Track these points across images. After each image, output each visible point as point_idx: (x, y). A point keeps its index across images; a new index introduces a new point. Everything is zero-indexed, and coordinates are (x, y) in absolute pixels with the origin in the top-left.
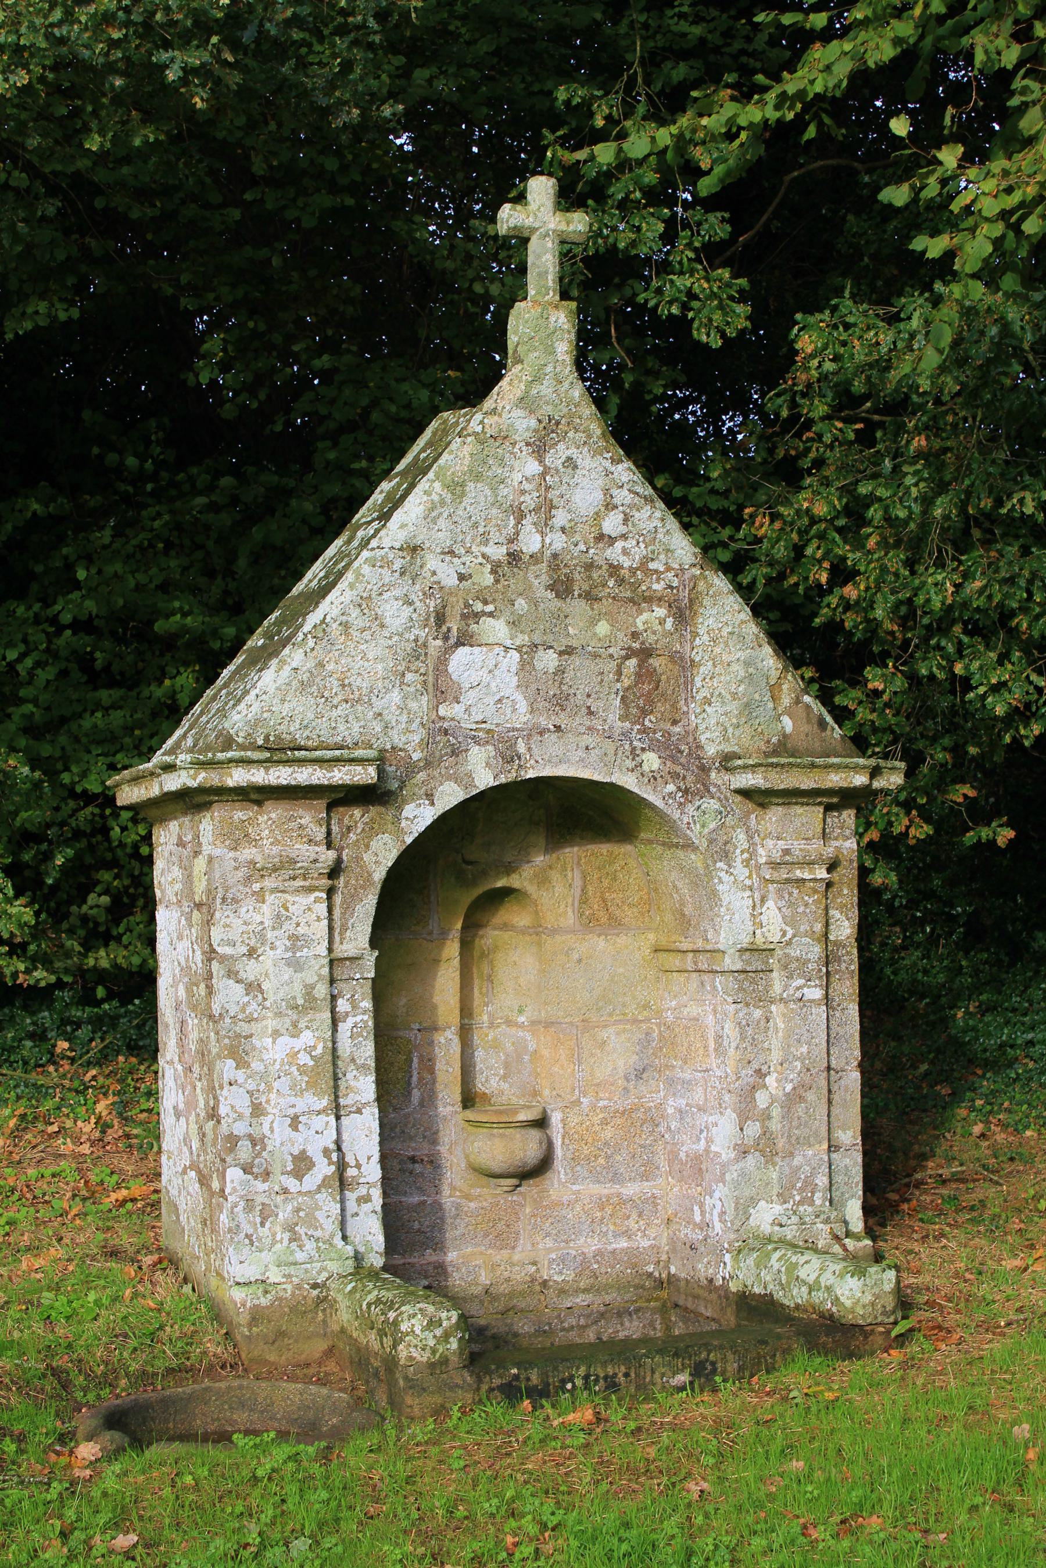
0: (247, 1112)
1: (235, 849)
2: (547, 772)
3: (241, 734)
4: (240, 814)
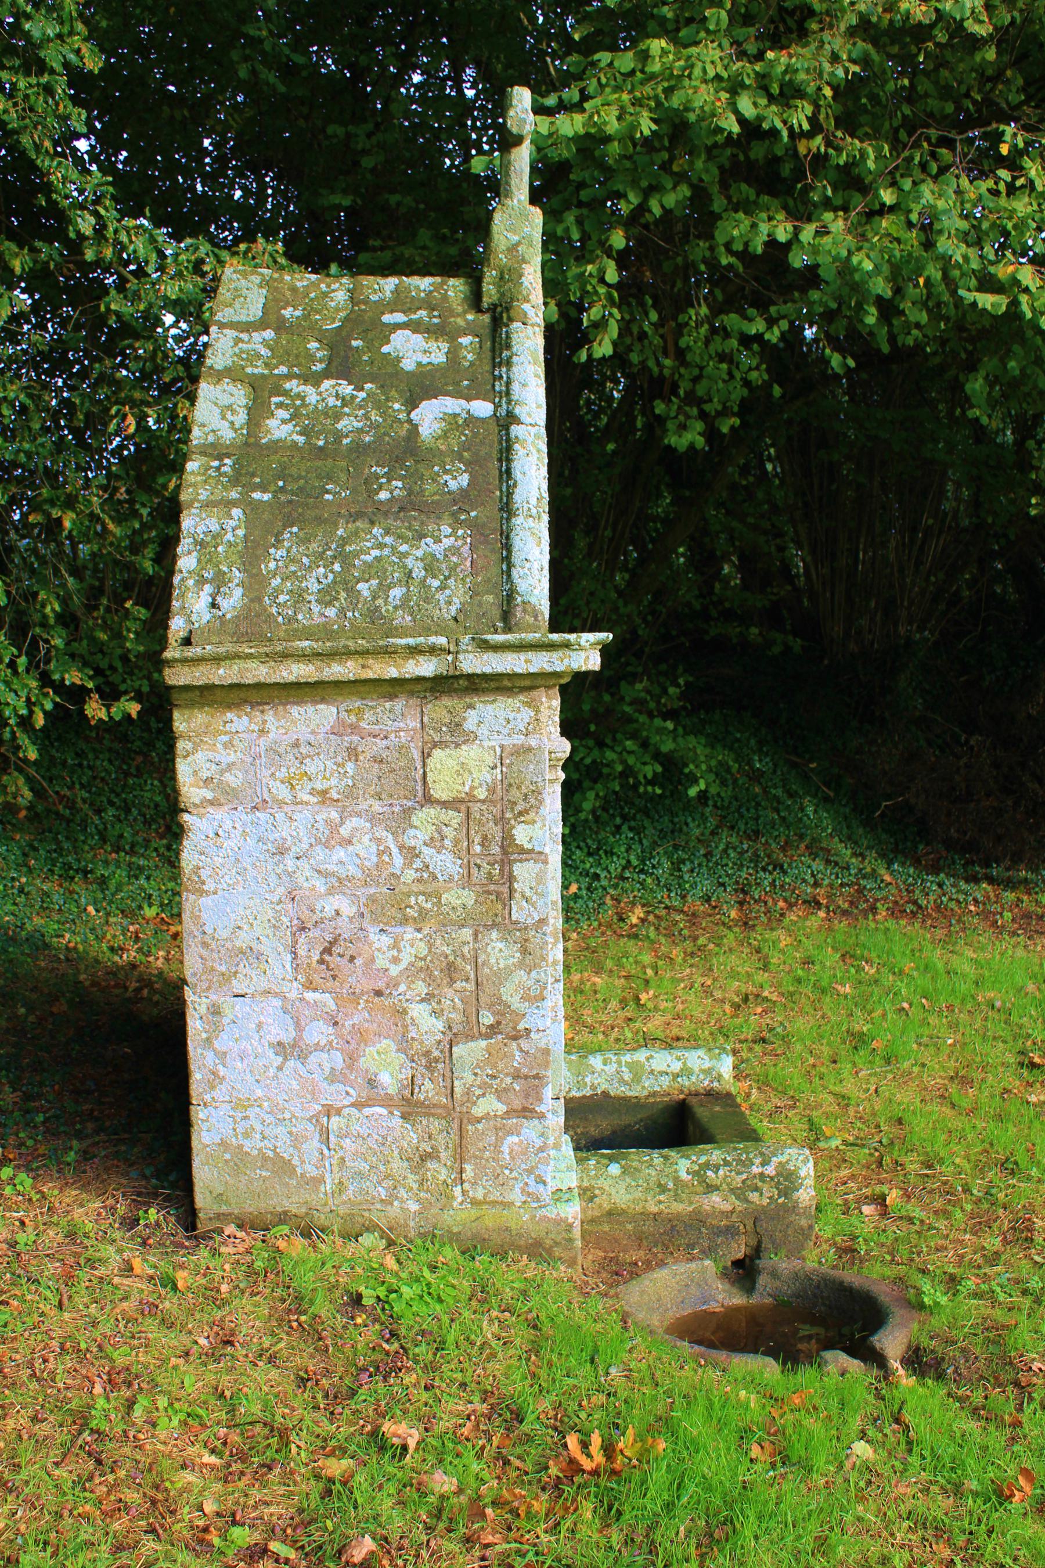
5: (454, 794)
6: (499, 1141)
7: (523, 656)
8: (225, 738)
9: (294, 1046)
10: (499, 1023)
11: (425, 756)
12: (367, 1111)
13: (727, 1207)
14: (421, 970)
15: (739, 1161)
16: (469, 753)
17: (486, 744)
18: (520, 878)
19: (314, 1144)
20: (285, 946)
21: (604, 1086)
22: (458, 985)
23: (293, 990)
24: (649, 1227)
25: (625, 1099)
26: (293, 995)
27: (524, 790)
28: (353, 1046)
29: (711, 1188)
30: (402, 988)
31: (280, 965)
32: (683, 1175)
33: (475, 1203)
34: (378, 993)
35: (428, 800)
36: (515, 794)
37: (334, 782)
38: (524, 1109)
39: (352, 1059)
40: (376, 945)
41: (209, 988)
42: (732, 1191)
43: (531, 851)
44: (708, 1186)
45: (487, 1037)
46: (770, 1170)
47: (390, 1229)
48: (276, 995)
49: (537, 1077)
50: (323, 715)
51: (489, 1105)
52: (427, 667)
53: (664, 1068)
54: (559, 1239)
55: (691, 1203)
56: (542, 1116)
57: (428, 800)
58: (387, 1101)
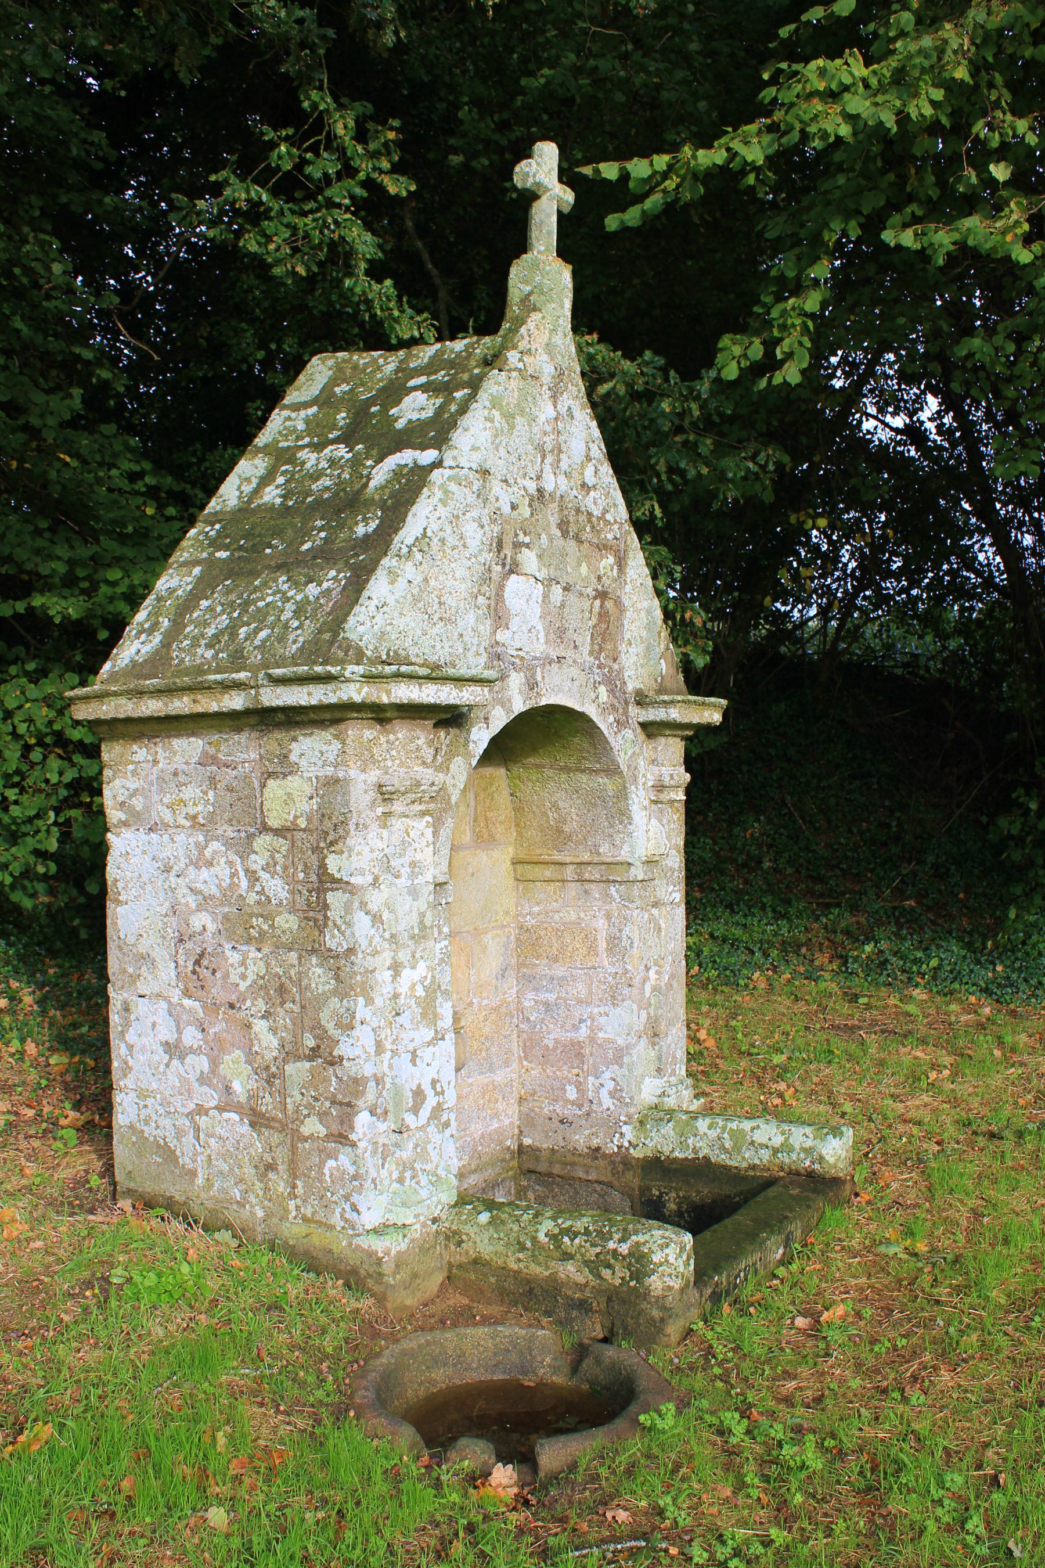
0: (372, 1050)
1: (364, 771)
2: (551, 702)
3: (371, 647)
4: (369, 732)
5: (282, 823)
6: (321, 1165)
7: (305, 689)
8: (131, 767)
9: (176, 1047)
10: (319, 1047)
11: (263, 786)
12: (226, 1115)
13: (580, 1279)
14: (259, 988)
15: (600, 1233)
16: (293, 783)
17: (305, 775)
18: (332, 907)
19: (189, 1138)
20: (171, 955)
21: (705, 1151)
22: (289, 1005)
23: (175, 995)
24: (509, 1284)
25: (727, 1168)
26: (175, 1000)
27: (334, 820)
28: (215, 1050)
29: (567, 1256)
30: (248, 1003)
31: (167, 972)
32: (542, 1237)
33: (305, 1219)
34: (232, 1006)
35: (265, 828)
36: (328, 825)
37: (200, 808)
38: (341, 1135)
39: (215, 1063)
40: (230, 961)
41: (123, 987)
42: (587, 1263)
43: (340, 881)
44: (565, 1253)
45: (310, 1059)
46: (624, 1249)
47: (243, 1230)
48: (165, 999)
49: (349, 1105)
50: (188, 748)
51: (313, 1126)
52: (236, 702)
53: (764, 1141)
54: (371, 1271)
55: (547, 1268)
56: (353, 1145)
57: (265, 828)
58: (238, 1108)
